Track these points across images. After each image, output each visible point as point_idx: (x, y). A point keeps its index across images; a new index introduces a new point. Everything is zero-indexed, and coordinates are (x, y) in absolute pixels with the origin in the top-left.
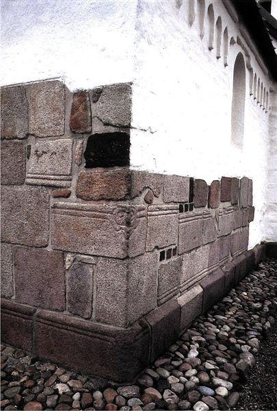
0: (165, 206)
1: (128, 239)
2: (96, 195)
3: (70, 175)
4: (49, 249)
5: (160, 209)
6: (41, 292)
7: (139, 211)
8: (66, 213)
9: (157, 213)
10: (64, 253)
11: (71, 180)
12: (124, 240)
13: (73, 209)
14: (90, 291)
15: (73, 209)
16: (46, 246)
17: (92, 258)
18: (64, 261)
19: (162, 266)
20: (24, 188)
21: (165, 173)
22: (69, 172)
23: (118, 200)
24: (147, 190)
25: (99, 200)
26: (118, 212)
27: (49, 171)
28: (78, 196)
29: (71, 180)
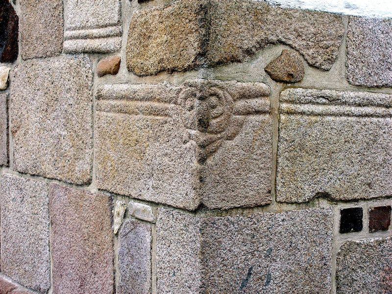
0: (351, 95)
1: (202, 160)
2: (151, 63)
3: (119, 23)
4: (93, 189)
5: (332, 101)
6: (83, 280)
7: (244, 96)
8: (112, 109)
9: (320, 109)
10: (114, 195)
11: (120, 34)
12: (195, 164)
13: (122, 98)
14: (147, 286)
15: (122, 98)
16: (89, 183)
17: (149, 208)
18: (112, 216)
19: (349, 248)
20: (59, 63)
21: (347, 12)
22: (116, 18)
23: (185, 70)
24: (280, 48)
25: (158, 73)
26: (186, 99)
27: (92, 21)
28: (130, 70)
29: (120, 34)
